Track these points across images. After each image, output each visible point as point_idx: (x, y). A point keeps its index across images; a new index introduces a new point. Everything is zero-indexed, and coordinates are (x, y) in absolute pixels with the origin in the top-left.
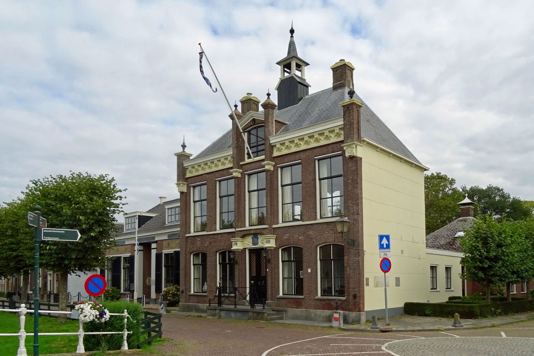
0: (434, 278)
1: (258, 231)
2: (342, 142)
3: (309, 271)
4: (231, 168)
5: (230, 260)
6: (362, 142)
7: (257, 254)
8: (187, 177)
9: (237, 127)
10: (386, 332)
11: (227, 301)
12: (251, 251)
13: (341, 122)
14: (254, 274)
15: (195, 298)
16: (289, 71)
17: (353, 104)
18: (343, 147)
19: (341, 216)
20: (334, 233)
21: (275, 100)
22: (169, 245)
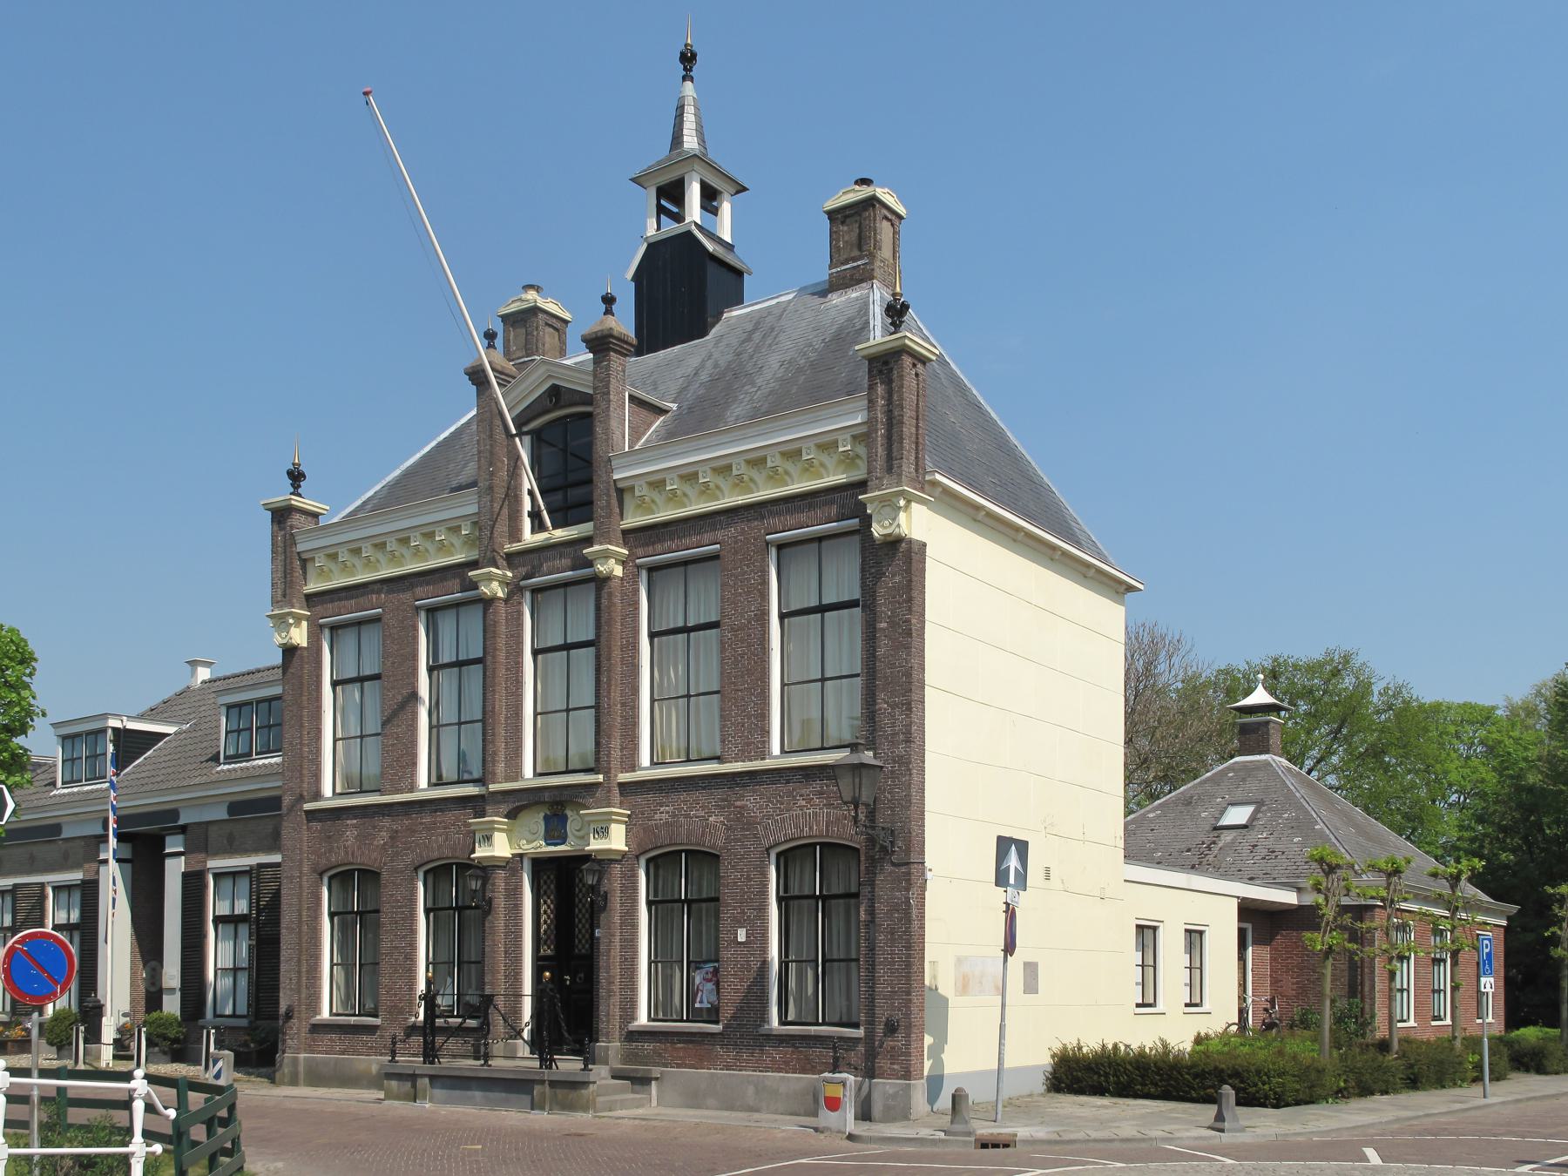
0: (1149, 966)
2: (862, 486)
3: (742, 936)
4: (474, 565)
10: (996, 1146)
11: (453, 1044)
12: (541, 866)
16: (675, 210)
17: (902, 351)
18: (863, 505)
19: (854, 747)
20: (829, 805)
21: (624, 323)
22: (231, 839)
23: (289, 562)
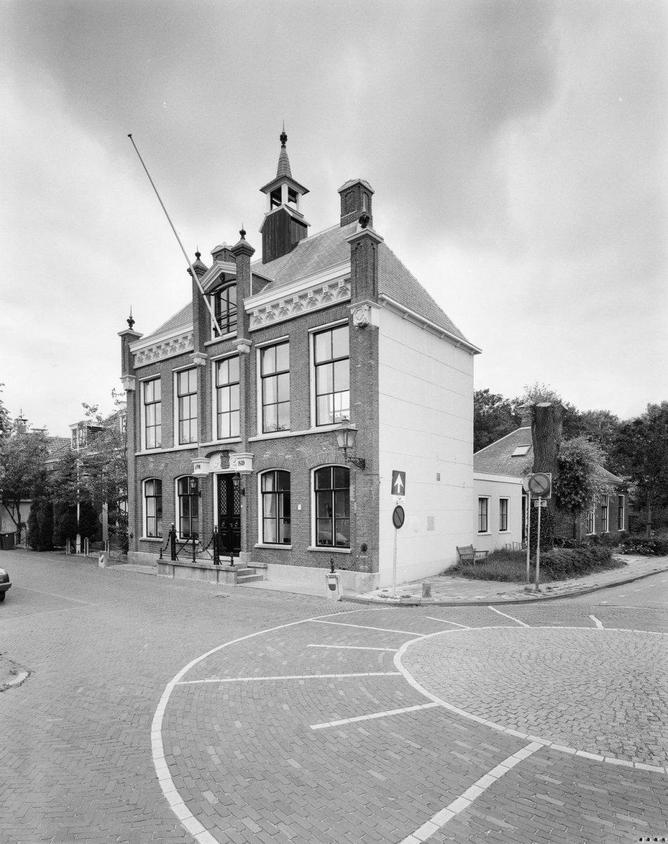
0: (484, 516)
1: (228, 448)
2: (349, 302)
3: (300, 508)
5: (191, 490)
6: (379, 302)
7: (228, 481)
8: (135, 367)
9: (199, 291)
13: (346, 269)
14: (224, 512)
15: (148, 545)
23: (128, 358)
